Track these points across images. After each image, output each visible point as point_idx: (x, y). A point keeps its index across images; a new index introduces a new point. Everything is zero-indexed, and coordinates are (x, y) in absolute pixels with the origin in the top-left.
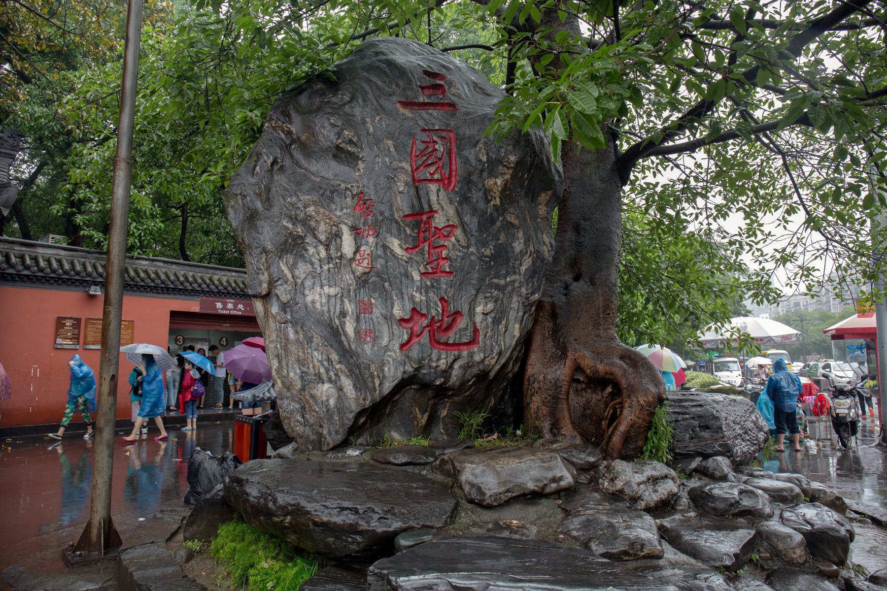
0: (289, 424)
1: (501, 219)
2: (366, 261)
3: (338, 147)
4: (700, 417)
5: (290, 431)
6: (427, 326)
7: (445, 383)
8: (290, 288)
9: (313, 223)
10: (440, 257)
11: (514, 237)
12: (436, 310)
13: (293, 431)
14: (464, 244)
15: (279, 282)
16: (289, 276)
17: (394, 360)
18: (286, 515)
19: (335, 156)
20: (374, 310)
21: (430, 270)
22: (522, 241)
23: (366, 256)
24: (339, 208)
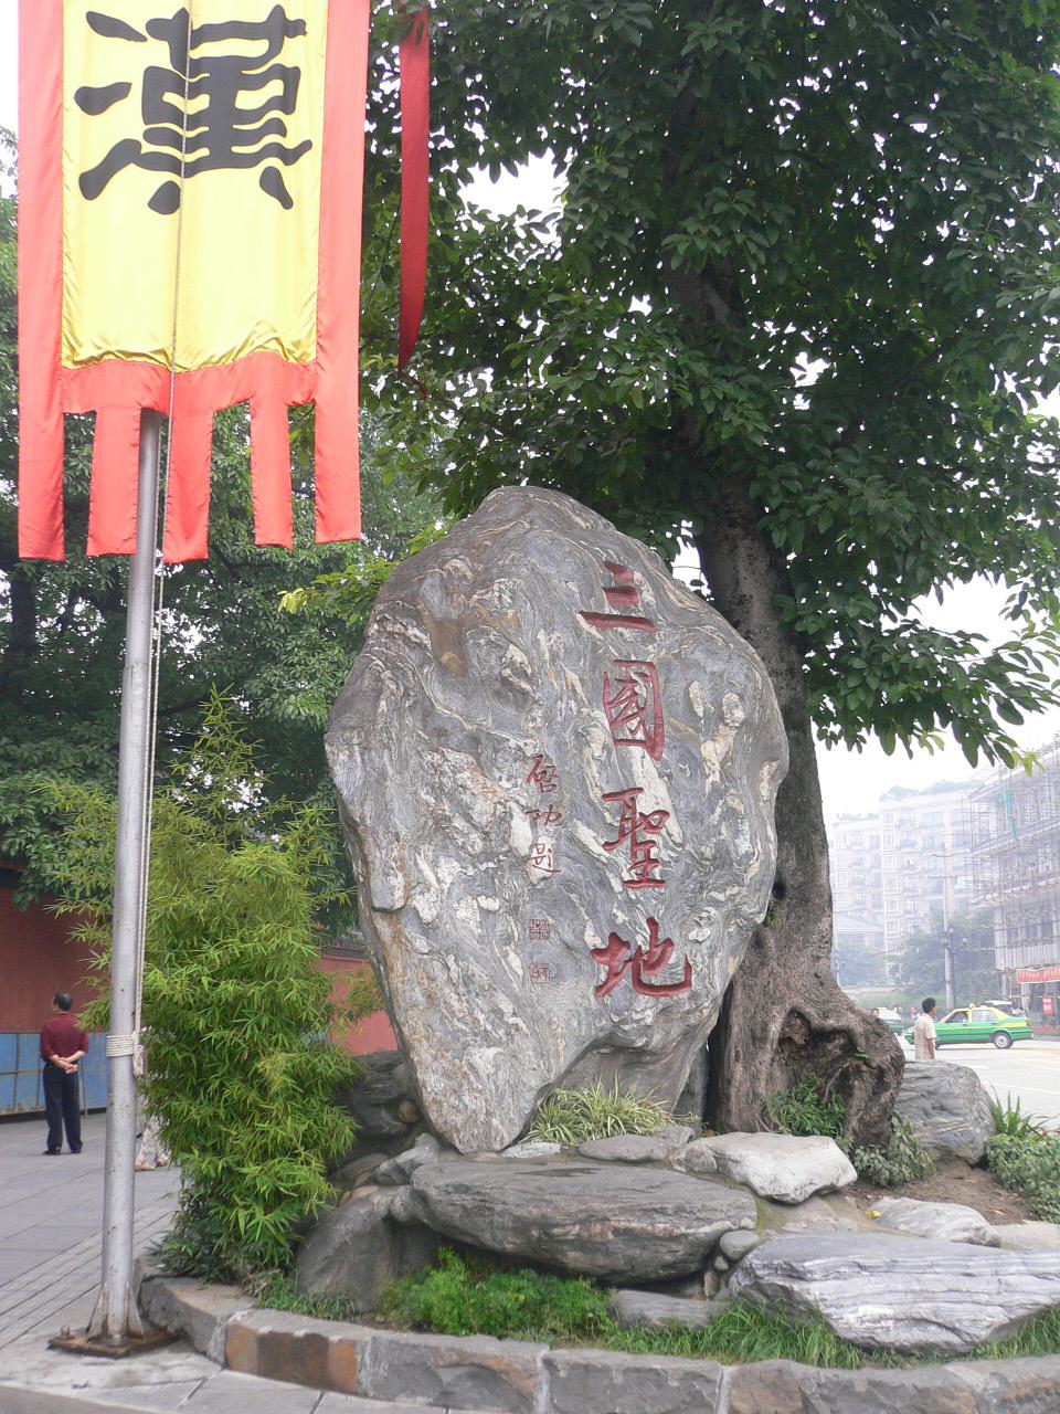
0: (439, 1111)
1: (721, 802)
2: (546, 861)
3: (505, 681)
4: (930, 1093)
5: (441, 1121)
6: (630, 960)
7: (647, 1044)
8: (434, 898)
9: (466, 798)
10: (649, 860)
11: (737, 833)
12: (641, 939)
13: (445, 1123)
14: (679, 840)
15: (418, 889)
16: (433, 880)
17: (586, 1010)
18: (574, 1225)
19: (497, 694)
20: (552, 935)
21: (635, 878)
22: (748, 837)
23: (546, 853)
24: (504, 777)
